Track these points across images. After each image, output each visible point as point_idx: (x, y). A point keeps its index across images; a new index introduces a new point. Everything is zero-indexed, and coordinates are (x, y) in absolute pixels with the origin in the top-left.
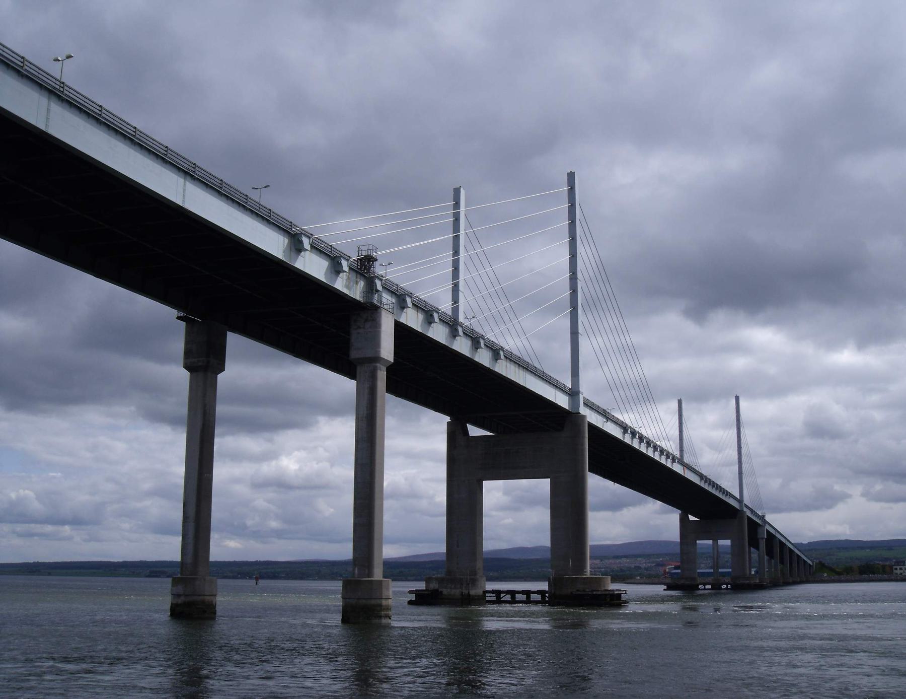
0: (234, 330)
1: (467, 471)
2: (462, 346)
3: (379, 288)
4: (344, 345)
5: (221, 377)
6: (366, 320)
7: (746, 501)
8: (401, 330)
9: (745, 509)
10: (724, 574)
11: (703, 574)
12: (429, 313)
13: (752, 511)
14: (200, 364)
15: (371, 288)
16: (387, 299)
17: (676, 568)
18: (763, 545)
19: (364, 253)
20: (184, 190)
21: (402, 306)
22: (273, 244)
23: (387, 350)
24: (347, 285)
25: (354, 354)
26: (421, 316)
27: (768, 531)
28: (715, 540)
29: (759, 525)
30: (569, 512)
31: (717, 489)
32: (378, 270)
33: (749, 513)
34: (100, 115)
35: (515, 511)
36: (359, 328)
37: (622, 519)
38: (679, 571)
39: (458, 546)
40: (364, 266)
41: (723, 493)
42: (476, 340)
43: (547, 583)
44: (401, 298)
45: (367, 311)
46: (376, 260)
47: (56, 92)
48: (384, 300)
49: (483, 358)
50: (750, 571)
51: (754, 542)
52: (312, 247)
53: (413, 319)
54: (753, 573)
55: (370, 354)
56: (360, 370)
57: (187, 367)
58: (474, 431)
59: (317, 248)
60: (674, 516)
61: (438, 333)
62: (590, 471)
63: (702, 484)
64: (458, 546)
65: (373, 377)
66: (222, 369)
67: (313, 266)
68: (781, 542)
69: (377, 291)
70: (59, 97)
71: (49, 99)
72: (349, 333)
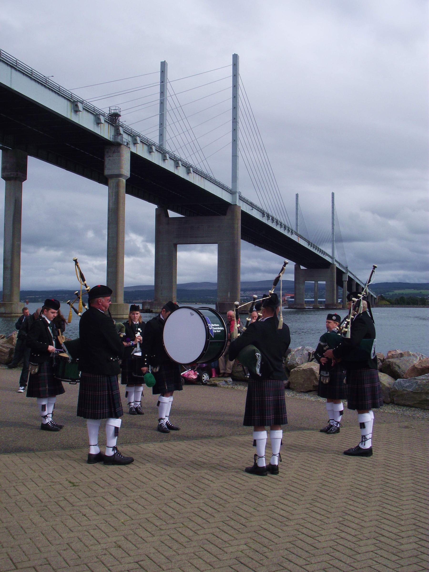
0: (31, 155)
1: (167, 241)
2: (169, 166)
3: (122, 132)
4: (101, 166)
5: (24, 183)
6: (114, 152)
7: (337, 257)
8: (135, 158)
9: (335, 263)
10: (321, 302)
11: (308, 302)
12: (150, 146)
13: (339, 264)
14: (12, 176)
15: (117, 133)
16: (126, 138)
17: (292, 298)
18: (345, 284)
19: (113, 111)
20: (11, 78)
21: (135, 143)
22: (61, 108)
23: (126, 170)
24: (105, 132)
25: (107, 172)
26: (146, 148)
27: (349, 276)
28: (316, 281)
29: (344, 273)
30: (229, 263)
31: (320, 252)
32: (121, 119)
33: (337, 265)
34: (16, 66)
35: (198, 262)
36: (110, 156)
37: (259, 264)
38: (293, 300)
39: (162, 283)
40: (114, 119)
41: (322, 253)
42: (176, 161)
43: (215, 305)
44: (134, 136)
45: (115, 146)
46: (120, 116)
47: (44, 83)
48: (124, 140)
49: (181, 172)
50: (337, 301)
51: (340, 283)
52: (84, 109)
53: (141, 151)
54: (339, 301)
55: (116, 172)
56: (111, 181)
57: (3, 177)
58: (172, 214)
59: (87, 110)
60: (291, 265)
61: (155, 158)
62: (242, 238)
63: (264, 220)
64: (162, 283)
65: (118, 185)
66: (25, 179)
67: (85, 121)
68: (357, 283)
69: (120, 134)
70: (15, 69)
71: (11, 70)
72: (103, 158)
